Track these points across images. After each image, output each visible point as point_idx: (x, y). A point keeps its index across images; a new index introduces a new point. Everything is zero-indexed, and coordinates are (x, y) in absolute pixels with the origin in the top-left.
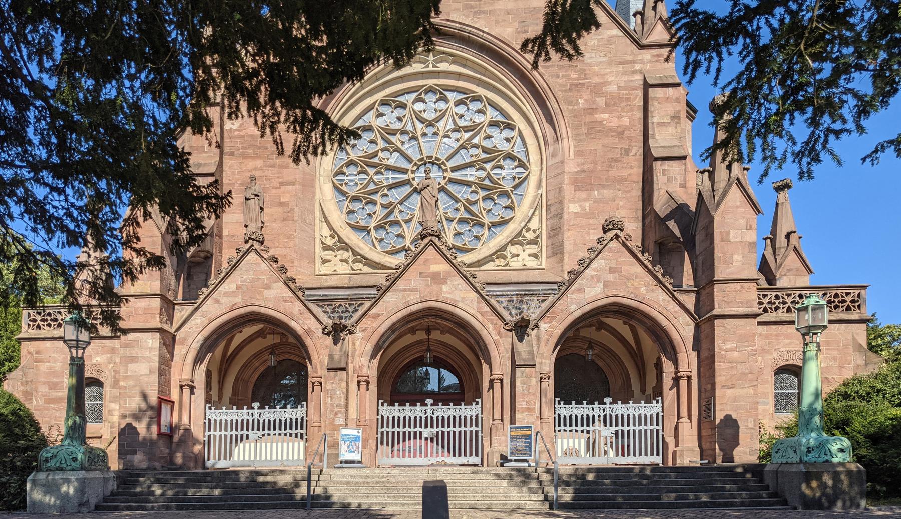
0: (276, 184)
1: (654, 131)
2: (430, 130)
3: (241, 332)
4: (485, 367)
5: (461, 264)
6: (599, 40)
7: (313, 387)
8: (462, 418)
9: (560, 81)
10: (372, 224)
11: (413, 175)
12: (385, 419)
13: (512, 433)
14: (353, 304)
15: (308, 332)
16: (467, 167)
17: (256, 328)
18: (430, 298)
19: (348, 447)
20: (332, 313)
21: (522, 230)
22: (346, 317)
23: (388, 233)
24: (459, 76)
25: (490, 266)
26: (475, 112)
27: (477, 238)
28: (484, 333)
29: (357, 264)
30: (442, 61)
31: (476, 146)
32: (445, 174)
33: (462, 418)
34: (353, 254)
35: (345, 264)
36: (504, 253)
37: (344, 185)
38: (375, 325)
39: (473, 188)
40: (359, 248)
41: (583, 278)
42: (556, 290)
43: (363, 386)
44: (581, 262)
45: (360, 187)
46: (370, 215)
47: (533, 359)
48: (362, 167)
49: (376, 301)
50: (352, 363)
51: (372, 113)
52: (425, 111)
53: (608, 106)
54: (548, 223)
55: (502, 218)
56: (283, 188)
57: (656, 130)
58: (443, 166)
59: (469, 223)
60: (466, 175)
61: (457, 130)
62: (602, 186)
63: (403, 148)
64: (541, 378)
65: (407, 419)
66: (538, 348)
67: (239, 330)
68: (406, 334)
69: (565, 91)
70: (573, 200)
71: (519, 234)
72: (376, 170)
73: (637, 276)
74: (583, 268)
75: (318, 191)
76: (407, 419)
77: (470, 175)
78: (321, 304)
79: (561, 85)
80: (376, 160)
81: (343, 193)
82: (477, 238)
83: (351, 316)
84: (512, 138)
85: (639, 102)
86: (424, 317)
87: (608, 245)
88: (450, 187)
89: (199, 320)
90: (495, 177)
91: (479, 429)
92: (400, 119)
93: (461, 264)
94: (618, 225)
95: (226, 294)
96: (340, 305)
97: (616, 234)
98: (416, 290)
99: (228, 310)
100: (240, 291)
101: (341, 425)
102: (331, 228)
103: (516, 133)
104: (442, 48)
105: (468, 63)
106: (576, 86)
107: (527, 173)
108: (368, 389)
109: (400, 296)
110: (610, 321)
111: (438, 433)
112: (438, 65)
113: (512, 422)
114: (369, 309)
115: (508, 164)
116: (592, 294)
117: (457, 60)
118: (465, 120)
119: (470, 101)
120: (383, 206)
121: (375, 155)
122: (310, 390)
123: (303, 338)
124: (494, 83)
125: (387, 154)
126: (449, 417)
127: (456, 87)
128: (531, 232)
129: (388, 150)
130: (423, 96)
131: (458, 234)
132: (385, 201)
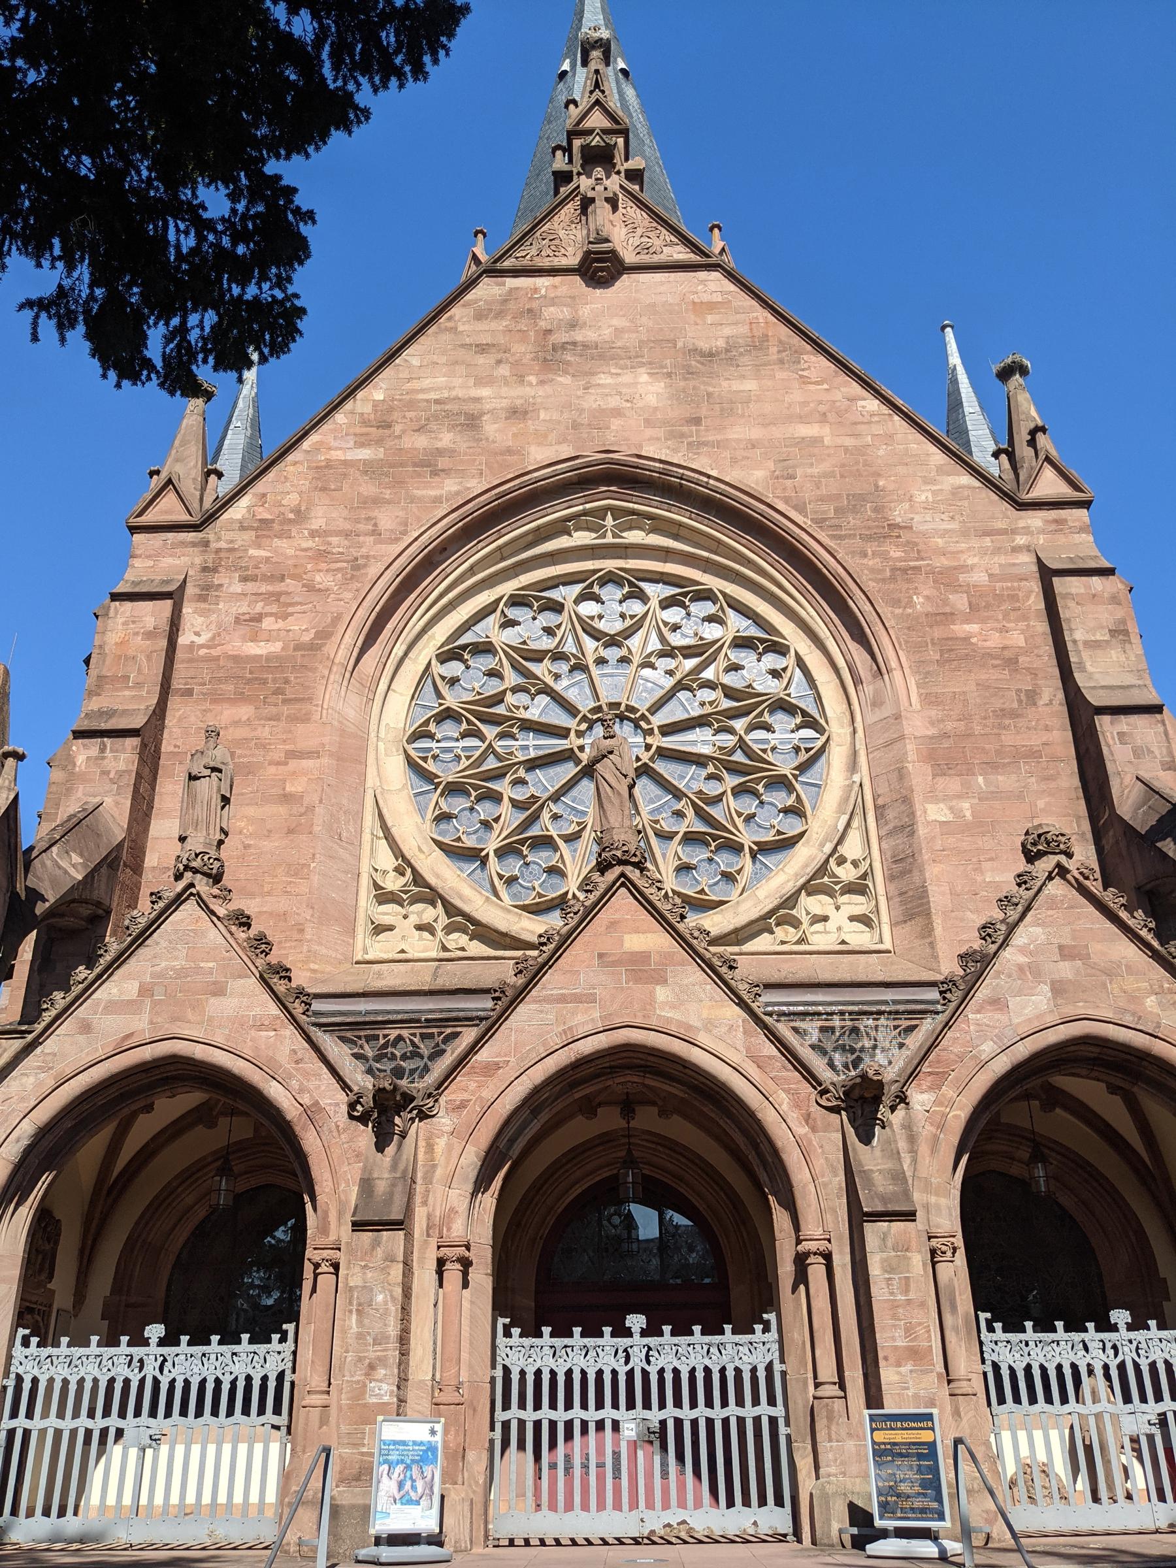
0: (279, 755)
1: (1080, 657)
2: (612, 654)
3: (149, 1108)
4: (781, 1218)
5: (696, 934)
6: (934, 493)
7: (316, 1276)
8: (730, 1374)
9: (871, 563)
10: (492, 844)
11: (580, 742)
12: (515, 1377)
13: (880, 1436)
14: (431, 1036)
15: (312, 1113)
16: (693, 727)
17: (191, 1099)
18: (627, 1020)
19: (401, 1485)
20: (378, 1059)
21: (827, 861)
22: (412, 1072)
23: (527, 864)
24: (666, 554)
25: (763, 942)
26: (704, 620)
27: (729, 877)
28: (768, 1117)
29: (455, 936)
30: (630, 529)
31: (710, 685)
32: (649, 740)
33: (730, 1374)
34: (447, 912)
35: (426, 934)
36: (794, 912)
37: (430, 761)
38: (488, 1094)
39: (711, 769)
40: (461, 897)
41: (999, 973)
42: (938, 1002)
43: (453, 1273)
44: (987, 931)
45: (465, 763)
46: (486, 825)
47: (907, 1195)
48: (469, 722)
49: (490, 1026)
50: (425, 1203)
51: (493, 620)
52: (601, 617)
53: (975, 611)
54: (884, 845)
55: (779, 833)
56: (293, 764)
57: (1085, 655)
58: (642, 723)
59: (708, 845)
60: (694, 743)
61: (669, 652)
62: (993, 766)
63: (559, 687)
64: (933, 1252)
65: (577, 1377)
66: (914, 1161)
67: (142, 1104)
68: (571, 1116)
69: (884, 580)
70: (933, 796)
71: (823, 869)
72: (499, 729)
73: (1128, 967)
74: (994, 948)
75: (371, 771)
76: (577, 1377)
77: (701, 741)
78: (349, 1034)
79: (872, 570)
80: (500, 710)
81: (428, 777)
82: (729, 877)
83: (426, 1069)
84: (784, 670)
85: (1037, 602)
86: (613, 1070)
87: (1045, 891)
88: (661, 767)
89: (32, 1079)
90: (755, 747)
91: (778, 1411)
92: (549, 631)
93: (696, 934)
94: (1059, 843)
95: (113, 1007)
96: (400, 1038)
97: (1059, 865)
98: (591, 999)
99: (109, 1050)
100: (148, 1001)
101: (382, 1408)
102: (398, 852)
103: (790, 661)
104: (631, 505)
105: (683, 532)
106: (905, 573)
107: (824, 739)
108: (465, 1284)
109: (551, 1013)
110: (1065, 1082)
111: (663, 1423)
112: (623, 534)
113: (874, 1398)
114: (473, 1049)
115: (780, 720)
116: (1029, 1011)
117: (659, 525)
118: (684, 636)
119: (691, 600)
120: (515, 804)
121: (498, 699)
122: (307, 1286)
123: (297, 1129)
124: (737, 567)
125: (523, 698)
126: (693, 1370)
127: (662, 573)
128: (848, 865)
129: (527, 691)
130: (596, 589)
131: (684, 868)
132: (520, 794)
